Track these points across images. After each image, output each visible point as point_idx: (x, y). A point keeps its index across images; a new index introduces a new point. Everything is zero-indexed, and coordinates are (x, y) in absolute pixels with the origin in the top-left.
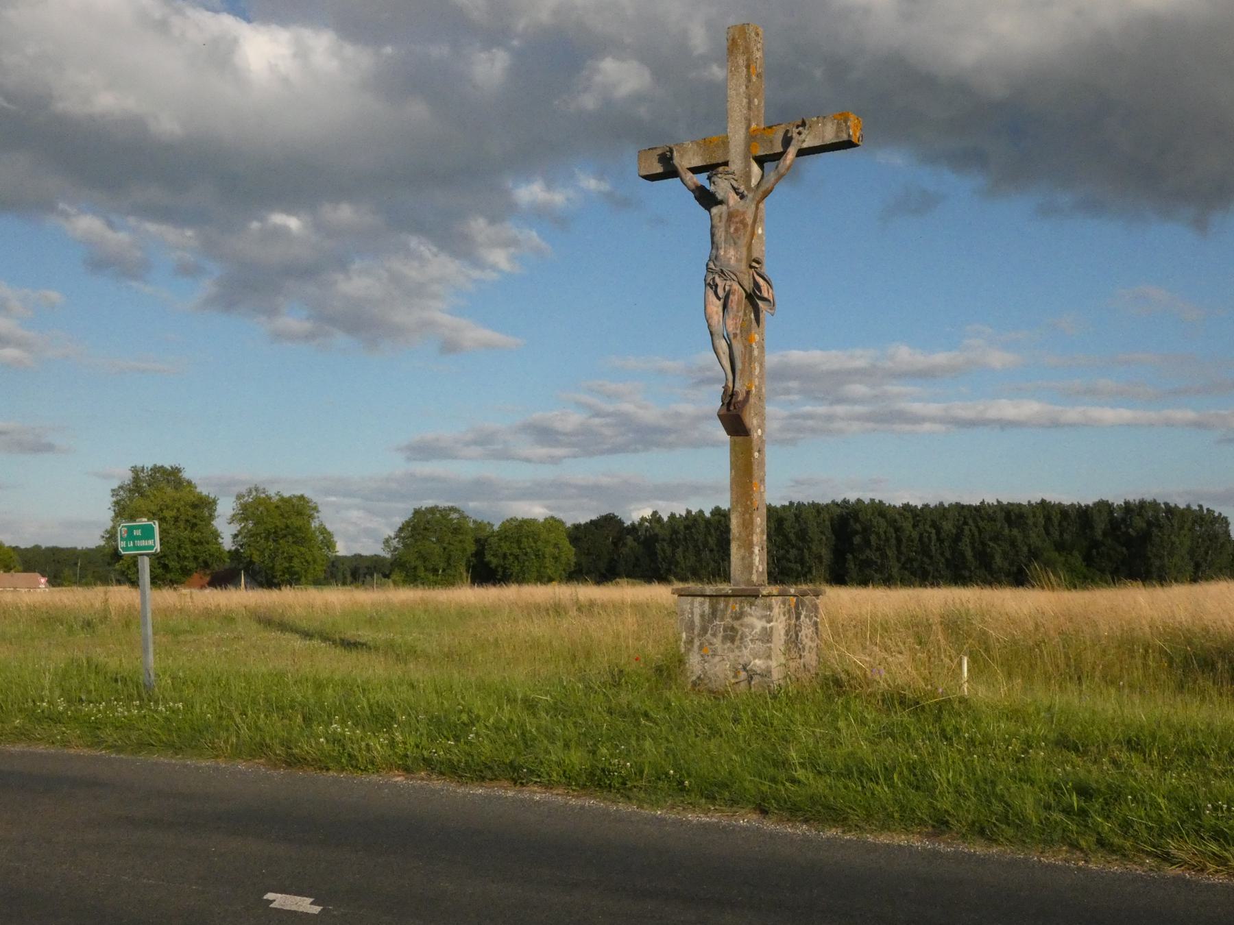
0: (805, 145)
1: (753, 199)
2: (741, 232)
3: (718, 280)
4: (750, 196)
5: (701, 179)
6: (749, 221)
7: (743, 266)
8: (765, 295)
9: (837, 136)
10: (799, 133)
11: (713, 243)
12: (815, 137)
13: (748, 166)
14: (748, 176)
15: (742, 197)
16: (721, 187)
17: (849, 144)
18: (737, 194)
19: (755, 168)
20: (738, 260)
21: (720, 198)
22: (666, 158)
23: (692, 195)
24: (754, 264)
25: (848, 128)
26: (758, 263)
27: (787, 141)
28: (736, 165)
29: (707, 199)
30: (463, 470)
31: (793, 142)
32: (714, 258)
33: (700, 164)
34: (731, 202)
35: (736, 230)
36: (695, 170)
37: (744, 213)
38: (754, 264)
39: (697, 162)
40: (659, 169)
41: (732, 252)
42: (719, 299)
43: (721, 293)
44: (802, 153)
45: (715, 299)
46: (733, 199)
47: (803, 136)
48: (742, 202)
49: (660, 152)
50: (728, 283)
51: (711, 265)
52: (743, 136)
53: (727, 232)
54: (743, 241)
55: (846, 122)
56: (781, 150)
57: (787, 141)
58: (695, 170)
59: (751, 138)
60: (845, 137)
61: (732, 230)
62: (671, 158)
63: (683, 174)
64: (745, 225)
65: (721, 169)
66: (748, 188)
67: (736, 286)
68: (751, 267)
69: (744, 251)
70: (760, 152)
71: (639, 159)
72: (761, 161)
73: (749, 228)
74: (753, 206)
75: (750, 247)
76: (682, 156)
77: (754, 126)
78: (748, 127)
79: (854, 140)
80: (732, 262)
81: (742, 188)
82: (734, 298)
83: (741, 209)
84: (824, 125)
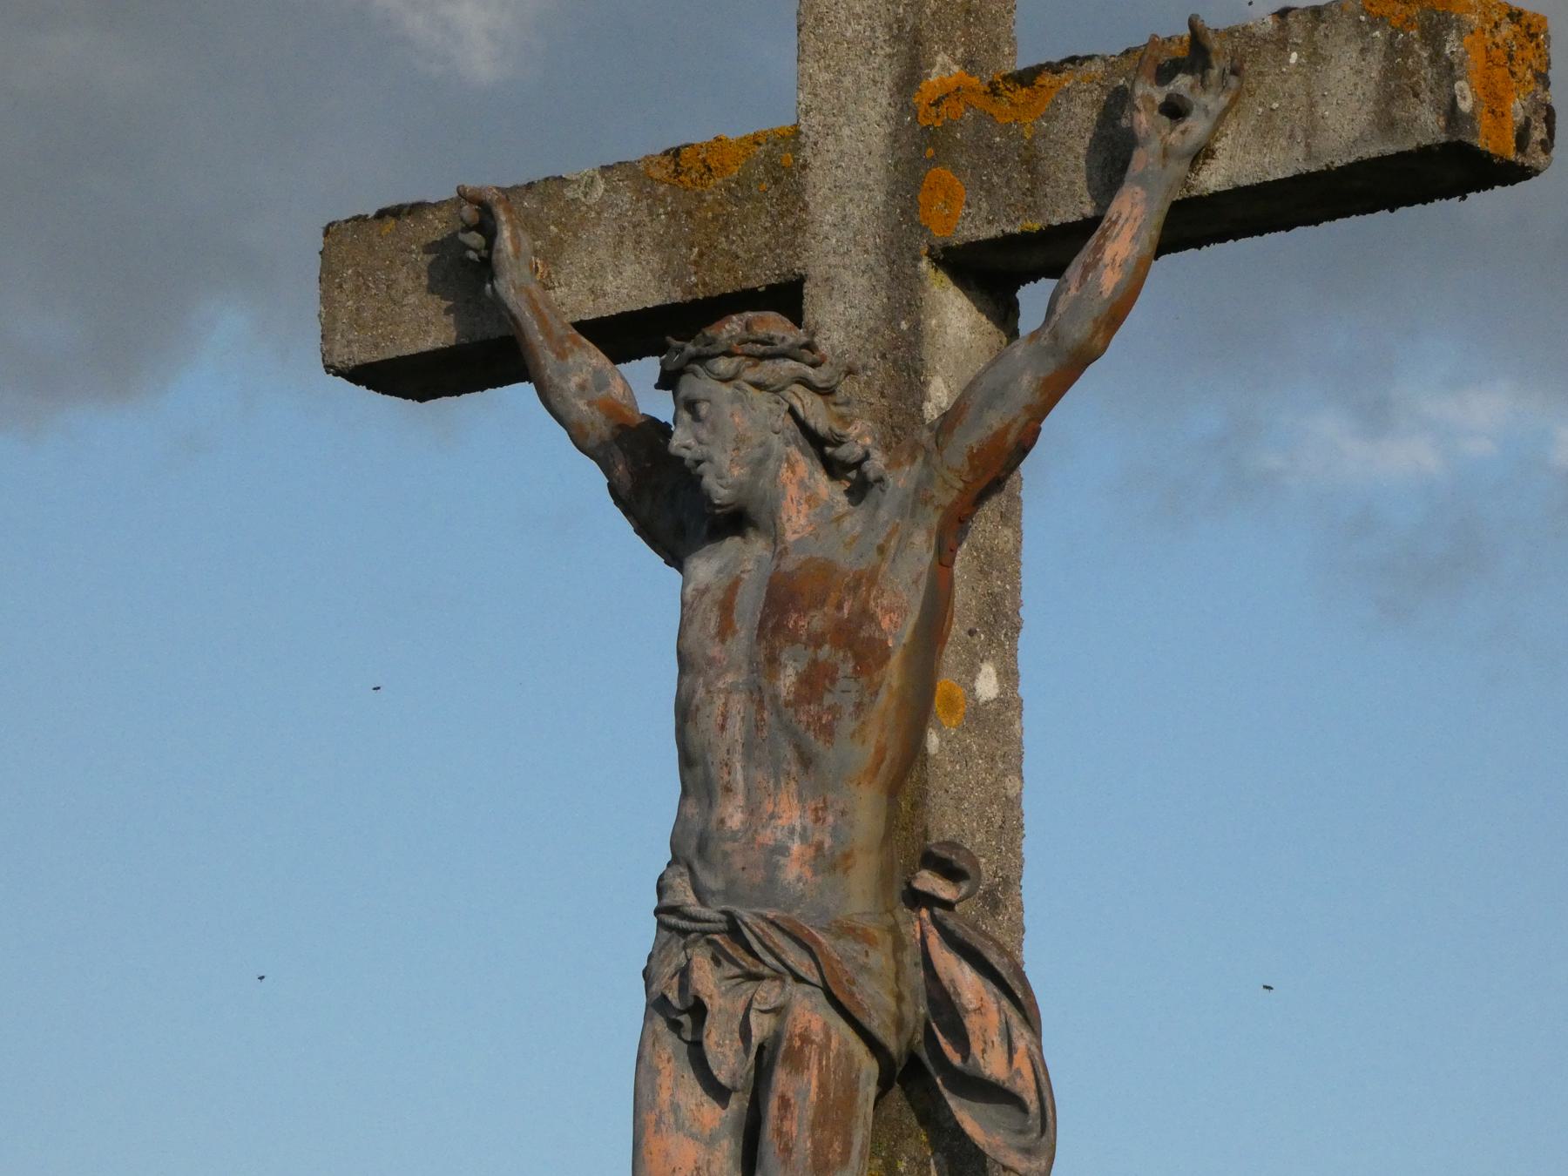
0: (1213, 179)
1: (920, 498)
2: (844, 693)
3: (708, 980)
4: (901, 480)
5: (640, 385)
6: (897, 627)
7: (858, 895)
8: (993, 1065)
9: (1387, 124)
10: (1175, 110)
11: (687, 760)
12: (1266, 128)
13: (905, 304)
14: (906, 360)
15: (861, 489)
16: (734, 429)
17: (1454, 168)
18: (834, 468)
19: (955, 316)
20: (830, 862)
21: (719, 490)
22: (464, 267)
23: (592, 479)
24: (929, 882)
25: (1449, 71)
26: (953, 874)
27: (1112, 158)
28: (842, 314)
29: (666, 499)
30: (796, 1112)
31: (1141, 160)
32: (692, 848)
33: (653, 299)
34: (796, 521)
35: (815, 681)
36: (620, 336)
37: (867, 580)
38: (929, 882)
39: (632, 285)
40: (430, 329)
41: (789, 814)
42: (718, 1092)
43: (727, 1058)
44: (1194, 223)
45: (692, 1095)
46: (804, 501)
47: (1197, 127)
48: (854, 522)
49: (437, 227)
50: (769, 993)
51: (684, 895)
52: (877, 137)
53: (758, 695)
54: (861, 745)
55: (1433, 36)
56: (1089, 210)
57: (1112, 158)
58: (620, 336)
59: (922, 145)
60: (1428, 127)
61: (787, 681)
62: (486, 268)
63: (548, 359)
64: (869, 656)
65: (732, 327)
66: (901, 424)
67: (811, 1015)
68: (917, 899)
69: (864, 810)
70: (975, 224)
71: (329, 275)
72: (991, 274)
73: (893, 673)
74: (921, 545)
75: (905, 773)
76: (552, 254)
77: (943, 69)
78: (909, 80)
79: (1493, 140)
80: (793, 871)
81: (860, 437)
82: (801, 1090)
83: (847, 561)
84: (1315, 57)
